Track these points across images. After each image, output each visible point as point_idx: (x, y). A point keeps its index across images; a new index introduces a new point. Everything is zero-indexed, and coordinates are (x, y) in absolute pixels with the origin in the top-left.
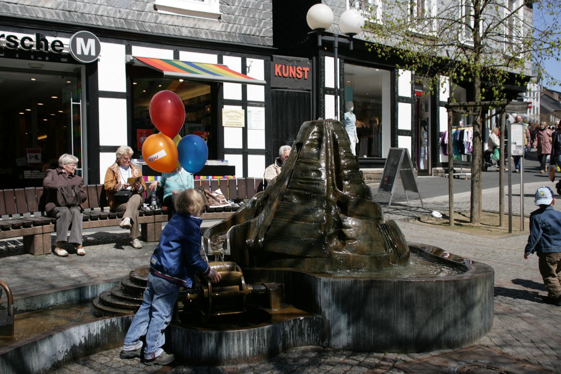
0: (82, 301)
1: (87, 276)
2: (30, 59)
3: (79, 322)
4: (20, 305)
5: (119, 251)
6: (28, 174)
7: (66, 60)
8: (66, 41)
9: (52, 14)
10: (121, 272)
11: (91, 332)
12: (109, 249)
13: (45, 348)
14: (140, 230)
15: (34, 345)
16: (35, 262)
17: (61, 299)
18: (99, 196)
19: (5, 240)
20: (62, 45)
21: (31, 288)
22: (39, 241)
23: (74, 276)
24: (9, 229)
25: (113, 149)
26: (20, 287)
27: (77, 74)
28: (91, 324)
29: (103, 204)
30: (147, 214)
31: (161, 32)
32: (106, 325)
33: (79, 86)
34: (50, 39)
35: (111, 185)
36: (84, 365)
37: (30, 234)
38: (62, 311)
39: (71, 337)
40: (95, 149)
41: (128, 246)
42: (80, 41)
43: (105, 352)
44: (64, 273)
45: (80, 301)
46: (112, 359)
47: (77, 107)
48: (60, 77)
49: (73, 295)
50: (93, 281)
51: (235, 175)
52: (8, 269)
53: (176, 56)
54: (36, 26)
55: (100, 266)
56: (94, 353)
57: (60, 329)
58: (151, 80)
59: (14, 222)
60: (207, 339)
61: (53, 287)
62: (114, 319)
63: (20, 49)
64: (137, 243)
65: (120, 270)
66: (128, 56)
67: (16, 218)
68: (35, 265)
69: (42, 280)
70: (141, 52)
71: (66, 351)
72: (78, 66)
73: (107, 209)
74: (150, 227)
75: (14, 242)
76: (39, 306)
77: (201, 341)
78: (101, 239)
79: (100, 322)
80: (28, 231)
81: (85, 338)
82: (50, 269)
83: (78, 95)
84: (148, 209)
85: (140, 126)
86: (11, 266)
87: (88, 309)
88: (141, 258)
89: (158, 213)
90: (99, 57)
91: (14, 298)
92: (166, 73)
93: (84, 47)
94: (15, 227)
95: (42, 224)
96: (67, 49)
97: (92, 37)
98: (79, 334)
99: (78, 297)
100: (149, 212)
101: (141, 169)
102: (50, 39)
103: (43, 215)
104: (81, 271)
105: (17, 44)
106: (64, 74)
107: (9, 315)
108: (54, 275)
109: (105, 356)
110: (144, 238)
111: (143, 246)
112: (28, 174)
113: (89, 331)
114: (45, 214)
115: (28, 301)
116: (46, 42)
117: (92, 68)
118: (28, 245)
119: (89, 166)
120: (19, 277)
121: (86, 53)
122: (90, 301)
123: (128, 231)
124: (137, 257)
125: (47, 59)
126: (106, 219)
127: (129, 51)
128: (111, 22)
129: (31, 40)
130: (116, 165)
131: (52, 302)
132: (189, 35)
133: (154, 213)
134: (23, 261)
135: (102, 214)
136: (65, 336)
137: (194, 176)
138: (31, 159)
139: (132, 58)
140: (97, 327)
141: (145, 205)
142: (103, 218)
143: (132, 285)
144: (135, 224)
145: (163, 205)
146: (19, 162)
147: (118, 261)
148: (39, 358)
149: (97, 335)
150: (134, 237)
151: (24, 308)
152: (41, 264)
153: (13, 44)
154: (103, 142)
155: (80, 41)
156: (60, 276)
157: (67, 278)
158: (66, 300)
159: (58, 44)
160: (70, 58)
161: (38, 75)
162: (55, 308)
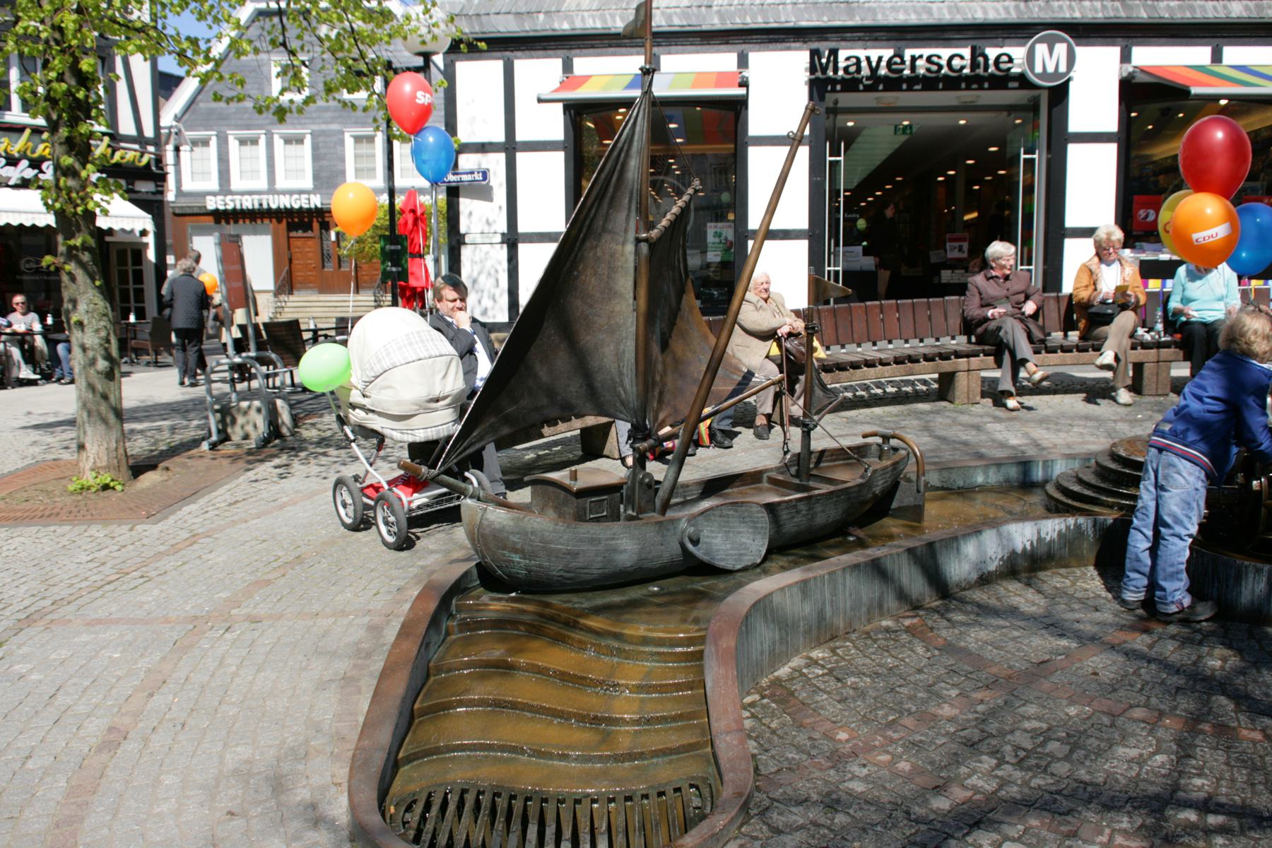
0: (1026, 484)
1: (1036, 444)
2: (959, 89)
3: (1023, 517)
4: (933, 478)
5: (1091, 407)
6: (946, 276)
7: (1016, 84)
8: (1018, 53)
9: (997, 11)
10: (1094, 443)
11: (1043, 535)
12: (1074, 402)
13: (970, 549)
14: (1131, 373)
15: (953, 541)
16: (955, 415)
17: (994, 477)
18: (1062, 312)
19: (912, 378)
20: (1011, 60)
21: (947, 455)
22: (962, 381)
23: (1014, 441)
24: (918, 361)
25: (1088, 232)
26: (931, 451)
27: (1034, 107)
28: (1044, 522)
29: (1068, 326)
30: (1145, 346)
31: (1188, 15)
32: (1068, 528)
33: (1036, 127)
34: (992, 53)
35: (1084, 295)
36: (1029, 585)
37: (950, 370)
38: (994, 495)
39: (1010, 539)
40: (1057, 233)
41: (1106, 401)
42: (1041, 49)
43: (1062, 571)
44: (999, 437)
45: (1023, 481)
46: (1074, 584)
47: (1030, 163)
48: (1005, 114)
49: (1013, 472)
50: (1045, 453)
51: (297, 363)
52: (915, 422)
53: (1217, 57)
54: (971, 34)
55: (1059, 431)
56: (1045, 569)
57: (994, 523)
58: (1165, 105)
59: (927, 351)
60: (1251, 576)
61: (981, 456)
62: (1081, 520)
63: (946, 76)
64: (1124, 396)
65: (1092, 439)
66: (1125, 66)
67: (928, 345)
68: (954, 420)
69: (965, 444)
70: (1150, 57)
71: (1002, 559)
72: (1036, 93)
73: (1074, 336)
74: (1148, 371)
75: (925, 382)
76: (961, 484)
77: (1238, 578)
78: (1062, 386)
79: (1057, 521)
80: (946, 366)
81: (1032, 544)
82: (977, 428)
83: (1034, 142)
84: (1148, 337)
85: (1140, 192)
86: (918, 418)
87: (1036, 498)
88: (1130, 422)
89: (1166, 345)
90: (1071, 74)
91: (927, 468)
92: (1195, 90)
93: (1046, 58)
94: (928, 358)
95: (968, 355)
96: (1019, 66)
97: (1062, 40)
98: (1023, 535)
99: (1021, 477)
100: (1148, 343)
101: (1137, 268)
102: (992, 53)
103: (969, 342)
104: (1026, 435)
105: (940, 67)
106: (1011, 109)
107: (918, 491)
108: (984, 437)
109: (1063, 576)
110: (1136, 387)
111: (1135, 402)
112: (946, 276)
113: (1039, 533)
114: (973, 339)
115: (945, 474)
116: (986, 58)
117: (1059, 94)
118: (945, 389)
119: (1045, 262)
120: (931, 436)
121: (1050, 69)
122: (1042, 485)
123: (1109, 375)
124: (1122, 420)
125: (986, 85)
126: (1071, 351)
127: (1126, 57)
128: (1096, 11)
129: (962, 58)
130: (1096, 259)
131: (980, 479)
132: (1245, 15)
133: (1159, 345)
134: (938, 412)
135: (1066, 343)
136: (1000, 535)
137: (1240, 278)
138: (954, 251)
139: (1131, 70)
140: (1052, 527)
141: (1140, 331)
142: (1066, 350)
143: (1113, 466)
144: (1122, 363)
145: (1175, 332)
146: (934, 257)
147: (1089, 424)
148: (960, 562)
149: (1052, 541)
150: (1119, 385)
151: (938, 484)
152: (964, 419)
153: (934, 68)
154: (1071, 221)
155: (1041, 49)
156: (993, 441)
157: (1003, 445)
158: (1001, 479)
159: (1005, 58)
160: (1023, 81)
161: (969, 115)
162: (983, 489)
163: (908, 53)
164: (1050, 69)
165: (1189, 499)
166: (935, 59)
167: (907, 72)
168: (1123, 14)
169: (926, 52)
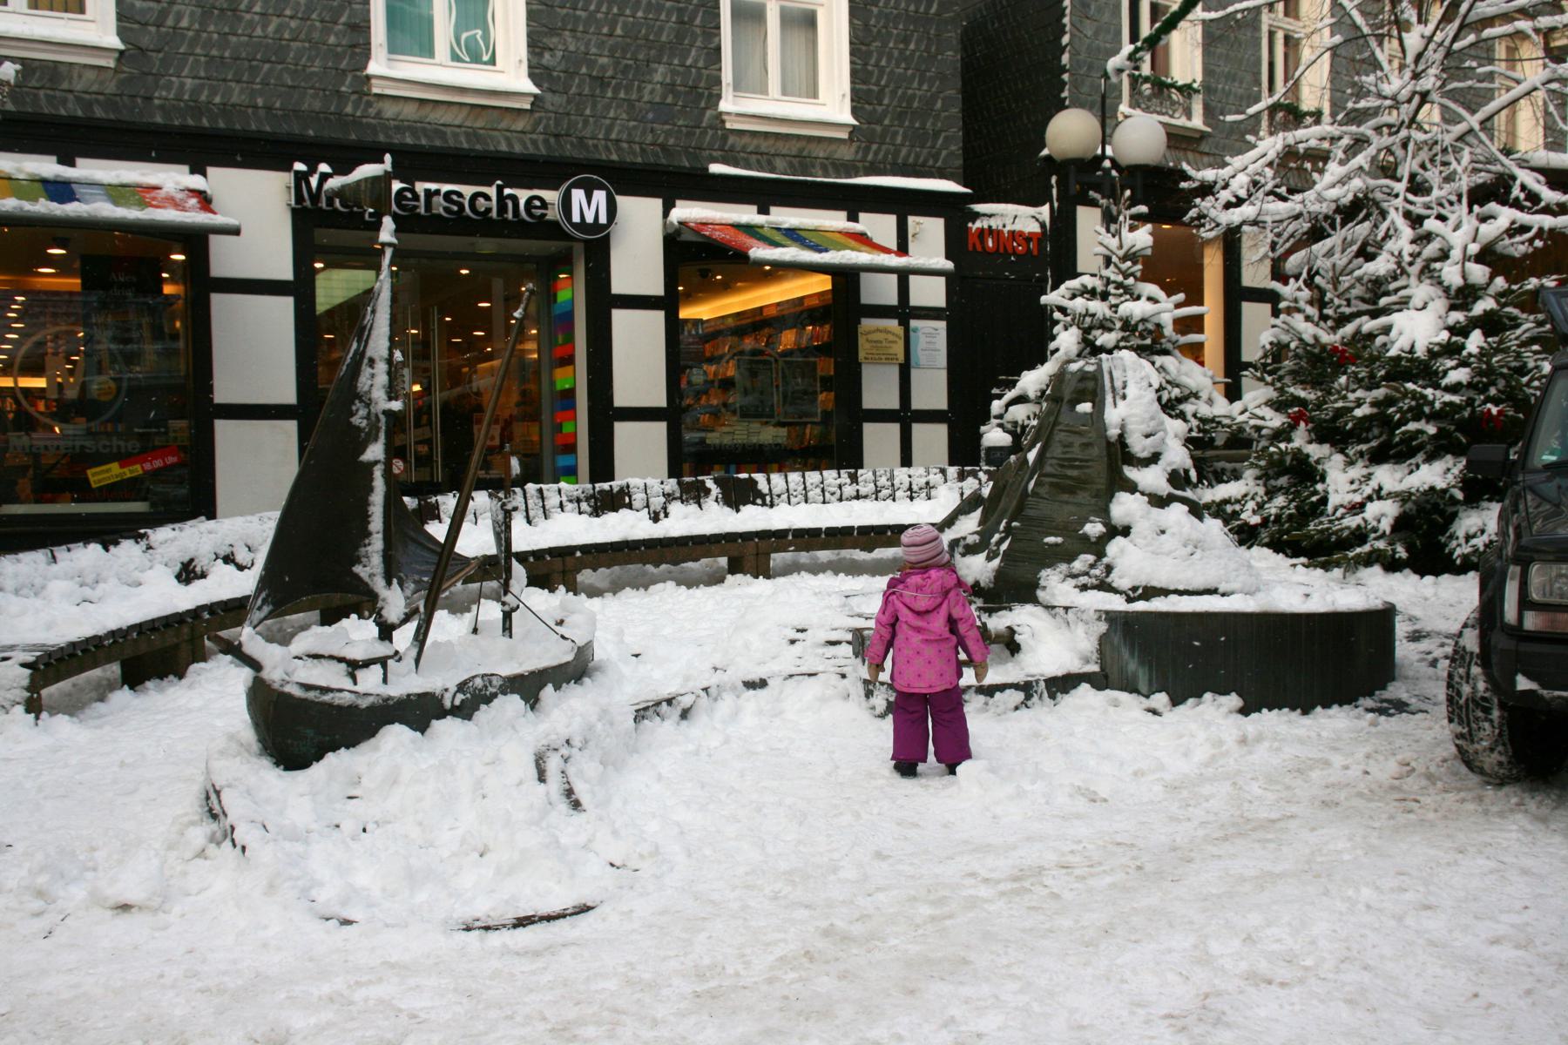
42: (578, 195)
97: (601, 187)
121: (590, 219)
127: (667, 208)
128: (634, 154)
129: (487, 198)
155: (578, 195)
159: (537, 203)
163: (421, 187)
164: (590, 219)
165: (1393, 333)
166: (455, 197)
167: (422, 211)
168: (664, 161)
169: (446, 188)
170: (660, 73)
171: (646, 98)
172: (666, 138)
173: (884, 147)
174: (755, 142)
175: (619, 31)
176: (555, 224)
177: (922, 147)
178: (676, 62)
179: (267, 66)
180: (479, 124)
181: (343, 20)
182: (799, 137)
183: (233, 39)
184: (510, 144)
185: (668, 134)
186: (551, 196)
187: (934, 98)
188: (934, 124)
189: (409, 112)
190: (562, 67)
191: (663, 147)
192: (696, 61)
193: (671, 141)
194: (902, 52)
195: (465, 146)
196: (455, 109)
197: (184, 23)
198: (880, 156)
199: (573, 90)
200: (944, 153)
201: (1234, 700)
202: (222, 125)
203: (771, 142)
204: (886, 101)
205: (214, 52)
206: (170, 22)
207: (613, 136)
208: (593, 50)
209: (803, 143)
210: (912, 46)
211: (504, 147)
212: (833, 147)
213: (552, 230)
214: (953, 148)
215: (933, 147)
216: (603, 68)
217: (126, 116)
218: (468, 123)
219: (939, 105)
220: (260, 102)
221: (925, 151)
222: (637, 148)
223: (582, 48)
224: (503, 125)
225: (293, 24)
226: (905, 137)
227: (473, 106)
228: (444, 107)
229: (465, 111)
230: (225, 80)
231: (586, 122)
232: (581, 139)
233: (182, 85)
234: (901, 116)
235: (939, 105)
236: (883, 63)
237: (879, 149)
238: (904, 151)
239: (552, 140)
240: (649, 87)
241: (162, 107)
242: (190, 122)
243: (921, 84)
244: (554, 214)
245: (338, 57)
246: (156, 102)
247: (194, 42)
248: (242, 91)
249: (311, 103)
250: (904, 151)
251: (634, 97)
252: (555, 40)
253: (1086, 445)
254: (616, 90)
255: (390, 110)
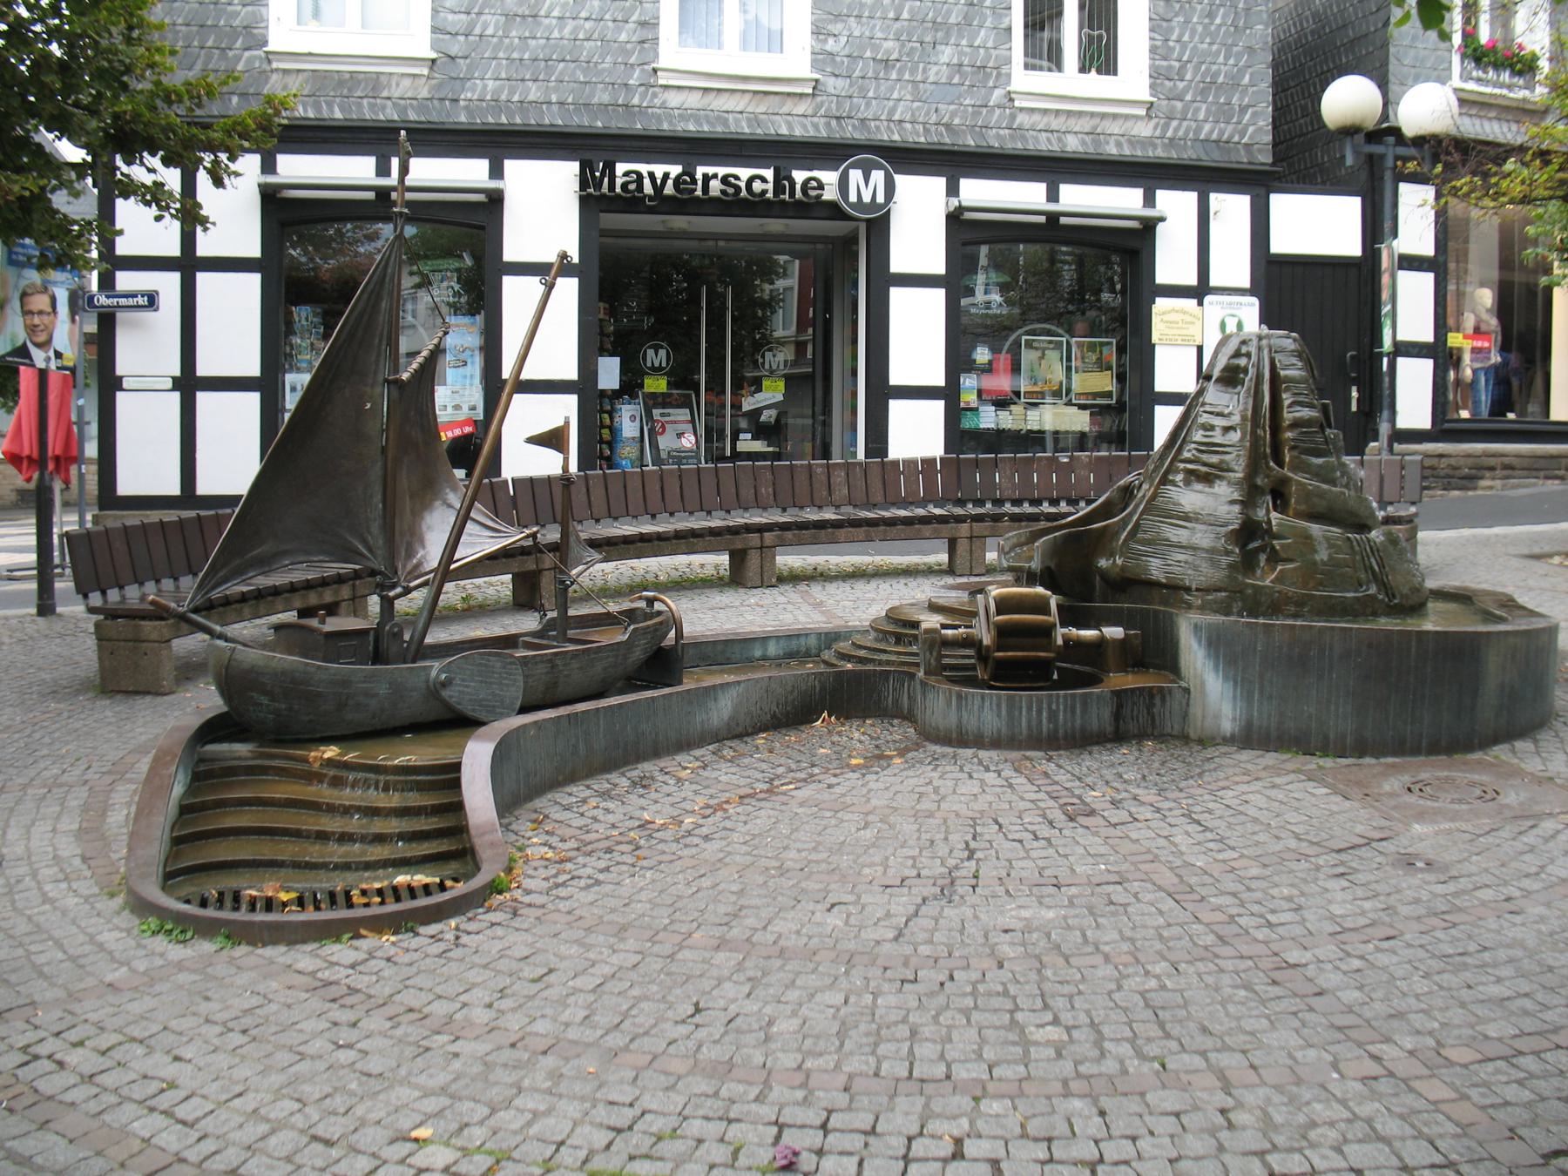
42: (856, 176)
97: (879, 167)
121: (867, 199)
127: (952, 190)
129: (764, 180)
155: (856, 176)
159: (814, 184)
163: (701, 171)
164: (867, 199)
167: (699, 193)
168: (947, 140)
169: (722, 171)
170: (946, 54)
171: (931, 79)
172: (951, 118)
173: (1185, 124)
174: (1045, 120)
175: (905, 15)
176: (833, 205)
177: (1228, 123)
178: (964, 42)
179: (562, 65)
180: (762, 109)
181: (634, 18)
182: (1092, 114)
183: (533, 43)
184: (790, 127)
185: (953, 114)
186: (829, 177)
187: (1241, 72)
188: (1241, 99)
189: (693, 100)
190: (846, 52)
191: (948, 126)
192: (985, 42)
193: (957, 121)
194: (1206, 27)
195: (747, 130)
196: (738, 96)
197: (490, 31)
198: (1181, 133)
199: (857, 73)
200: (1251, 129)
201: (178, 374)
202: (518, 121)
203: (1062, 119)
204: (1188, 77)
205: (515, 55)
206: (477, 31)
207: (896, 117)
208: (879, 35)
209: (1096, 121)
210: (1218, 21)
211: (784, 131)
212: (1129, 124)
213: (834, 211)
214: (1261, 123)
215: (1239, 123)
216: (889, 52)
217: (434, 117)
218: (750, 109)
219: (1246, 80)
220: (554, 99)
221: (1230, 128)
222: (920, 128)
223: (867, 33)
224: (785, 110)
225: (588, 25)
226: (1208, 111)
227: (755, 92)
228: (727, 95)
229: (748, 97)
230: (523, 80)
231: (868, 105)
232: (863, 120)
233: (485, 86)
234: (1204, 92)
235: (1246, 80)
236: (1186, 38)
237: (1180, 126)
238: (1207, 127)
239: (834, 123)
240: (934, 69)
241: (466, 108)
242: (491, 120)
243: (1227, 58)
244: (830, 194)
245: (629, 53)
246: (462, 103)
247: (497, 48)
248: (538, 89)
249: (602, 96)
250: (1207, 127)
251: (919, 78)
252: (840, 26)
253: (1227, 429)
254: (901, 72)
255: (674, 99)
